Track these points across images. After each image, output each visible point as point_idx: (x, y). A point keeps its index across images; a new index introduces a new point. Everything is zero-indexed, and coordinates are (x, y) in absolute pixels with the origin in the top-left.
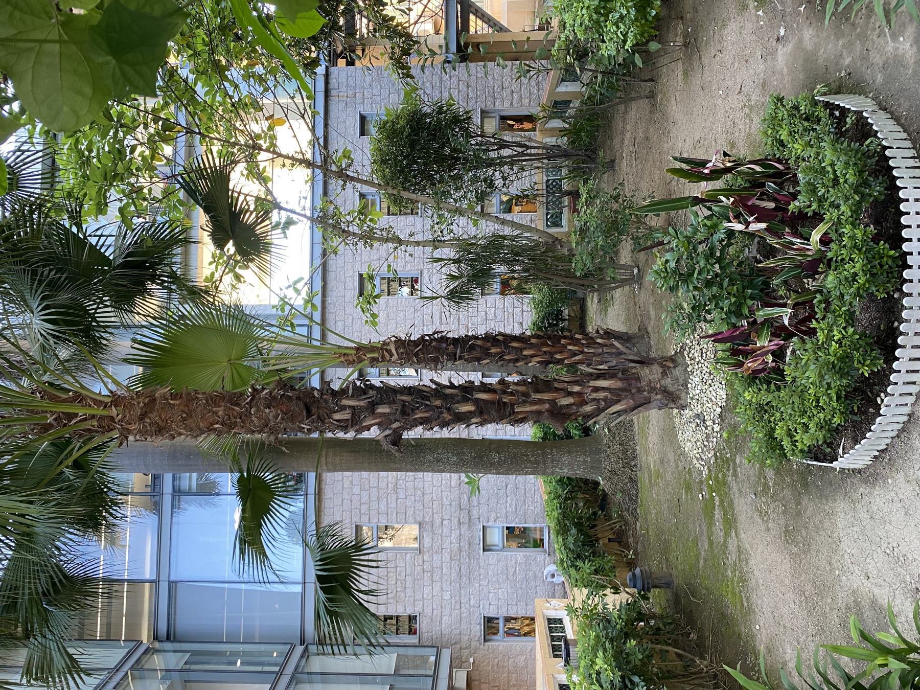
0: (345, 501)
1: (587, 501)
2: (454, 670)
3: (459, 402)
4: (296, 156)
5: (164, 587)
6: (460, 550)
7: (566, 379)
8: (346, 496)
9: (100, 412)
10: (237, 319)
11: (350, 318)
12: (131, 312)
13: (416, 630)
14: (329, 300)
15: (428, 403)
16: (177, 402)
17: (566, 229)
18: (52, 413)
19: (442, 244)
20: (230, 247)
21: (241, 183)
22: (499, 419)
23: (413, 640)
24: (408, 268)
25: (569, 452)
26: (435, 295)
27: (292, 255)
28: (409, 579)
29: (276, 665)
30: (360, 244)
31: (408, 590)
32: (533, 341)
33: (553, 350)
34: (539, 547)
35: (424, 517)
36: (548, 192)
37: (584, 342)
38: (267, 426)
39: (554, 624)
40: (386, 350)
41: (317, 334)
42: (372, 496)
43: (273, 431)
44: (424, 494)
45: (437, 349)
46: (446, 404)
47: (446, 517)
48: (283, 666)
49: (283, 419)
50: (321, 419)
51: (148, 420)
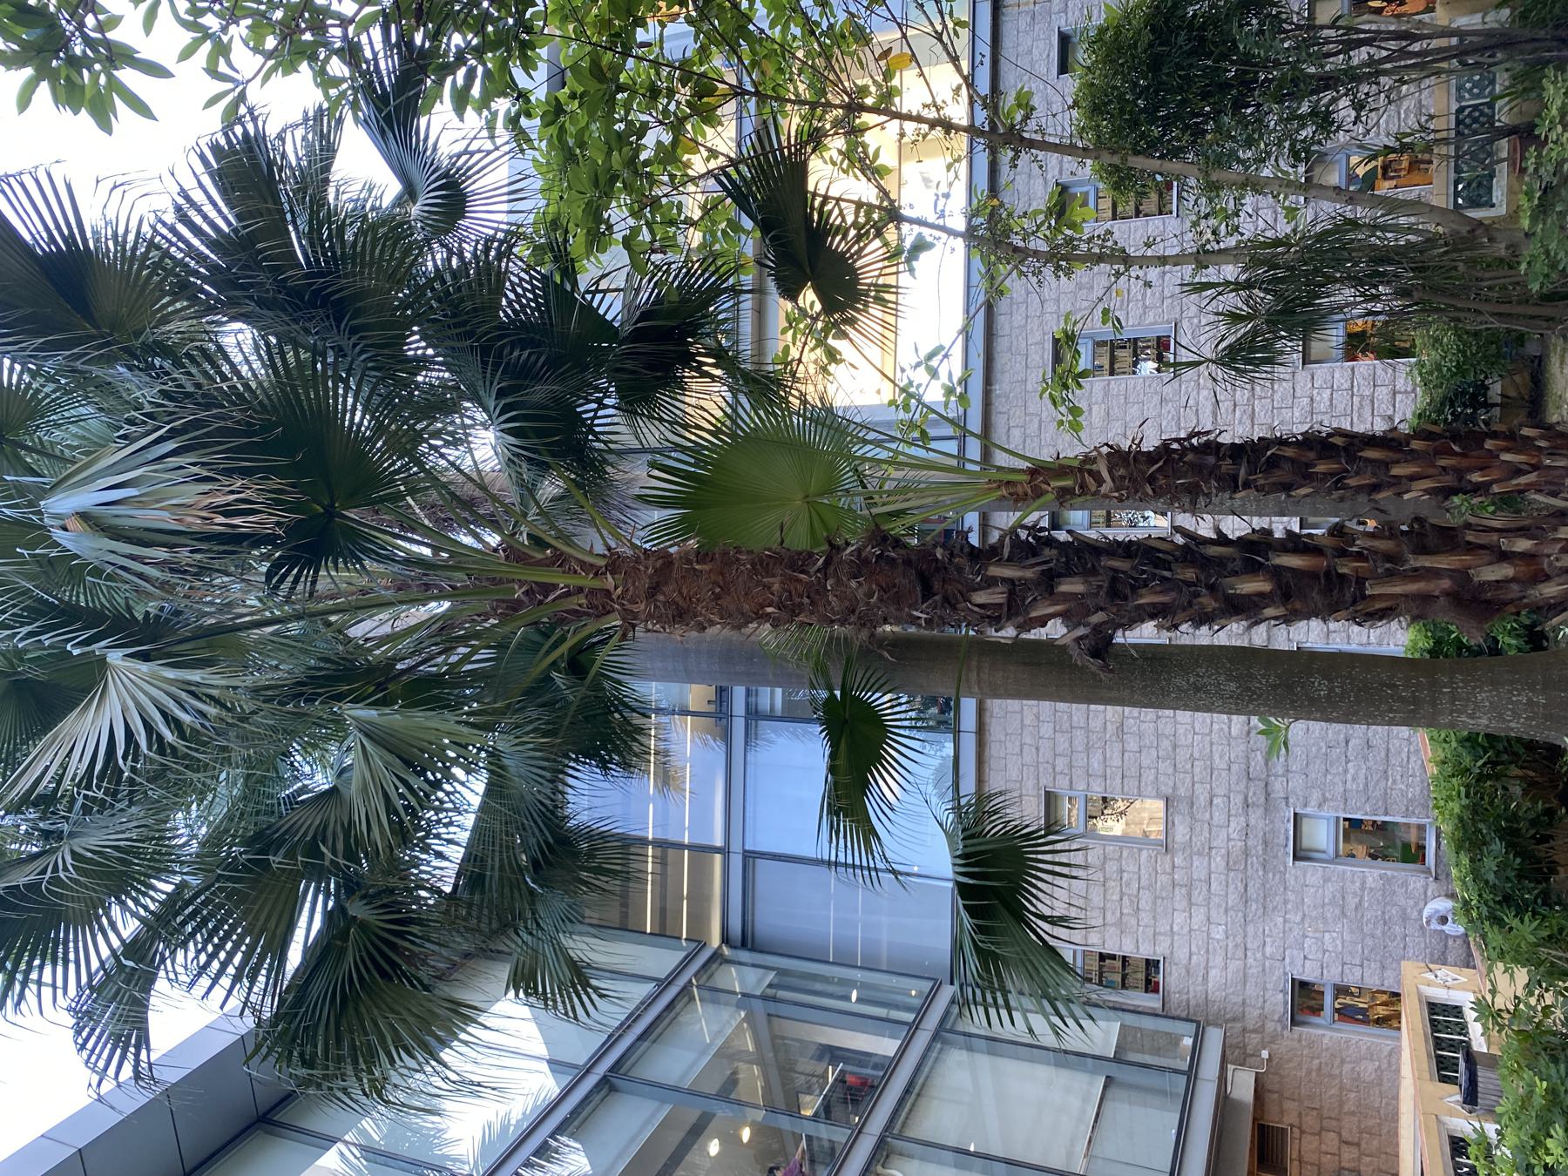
0: (1026, 748)
1: (1530, 786)
2: (1231, 1067)
3: (1235, 573)
4: (926, 113)
5: (736, 861)
6: (1246, 853)
7: (1496, 524)
8: (1028, 740)
9: (588, 582)
10: (823, 425)
11: (1036, 420)
12: (650, 417)
13: (1157, 983)
14: (997, 389)
15: (1167, 574)
16: (706, 567)
17: (1501, 210)
18: (522, 583)
19: (1213, 258)
20: (809, 297)
21: (825, 175)
22: (1327, 611)
23: (1152, 1002)
24: (1150, 318)
25: (1494, 684)
26: (1196, 358)
27: (930, 301)
28: (1146, 897)
29: (908, 1009)
30: (1048, 271)
31: (1142, 915)
32: (1416, 445)
33: (1465, 463)
34: (1414, 862)
35: (1175, 788)
36: (1458, 133)
37: (1542, 444)
38: (853, 612)
39: (1442, 1016)
40: (1090, 472)
41: (974, 450)
42: (1076, 742)
43: (868, 622)
44: (1175, 747)
45: (1197, 468)
46: (1209, 576)
47: (1221, 791)
48: (922, 1012)
49: (881, 599)
50: (949, 602)
51: (661, 598)
